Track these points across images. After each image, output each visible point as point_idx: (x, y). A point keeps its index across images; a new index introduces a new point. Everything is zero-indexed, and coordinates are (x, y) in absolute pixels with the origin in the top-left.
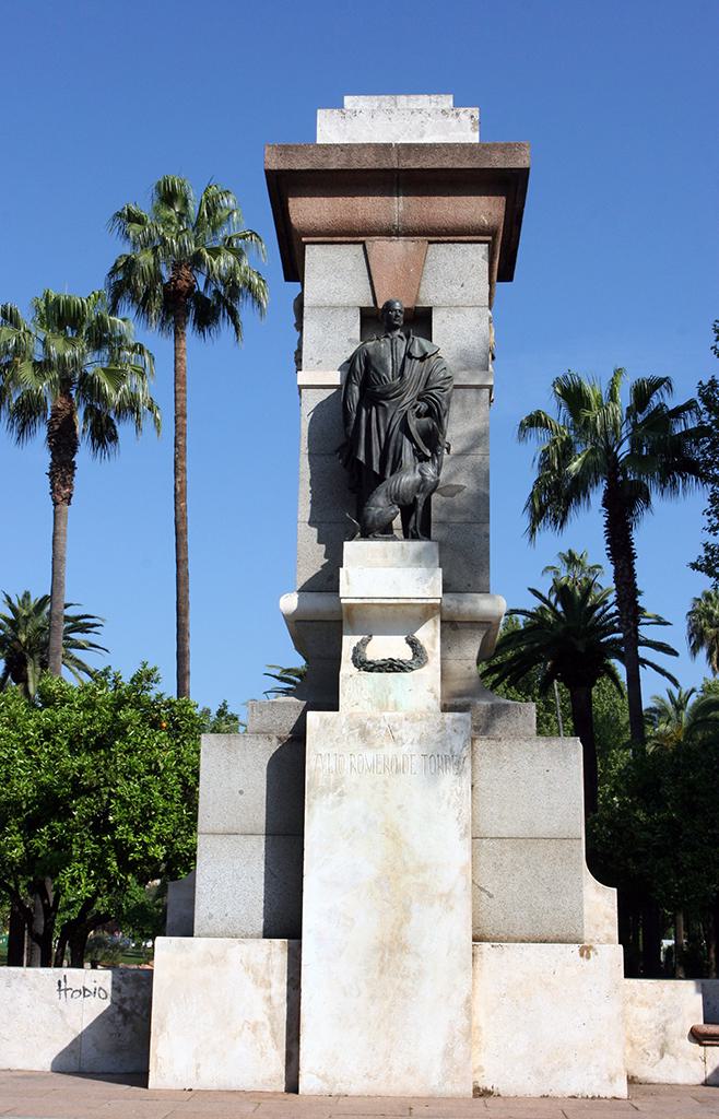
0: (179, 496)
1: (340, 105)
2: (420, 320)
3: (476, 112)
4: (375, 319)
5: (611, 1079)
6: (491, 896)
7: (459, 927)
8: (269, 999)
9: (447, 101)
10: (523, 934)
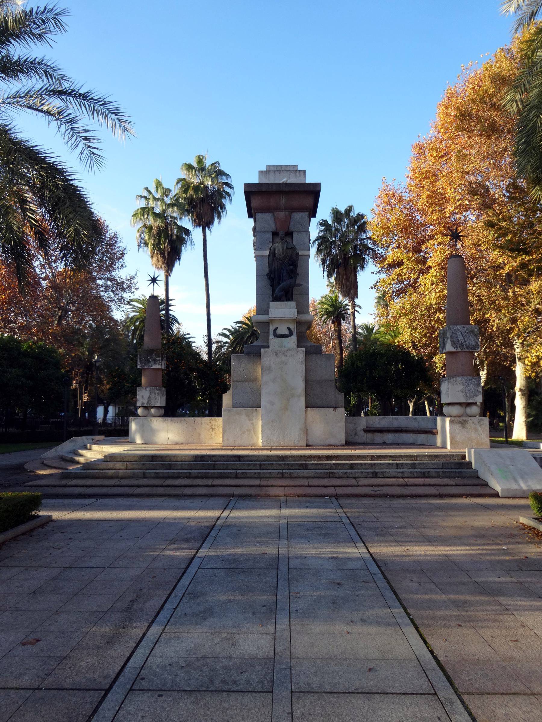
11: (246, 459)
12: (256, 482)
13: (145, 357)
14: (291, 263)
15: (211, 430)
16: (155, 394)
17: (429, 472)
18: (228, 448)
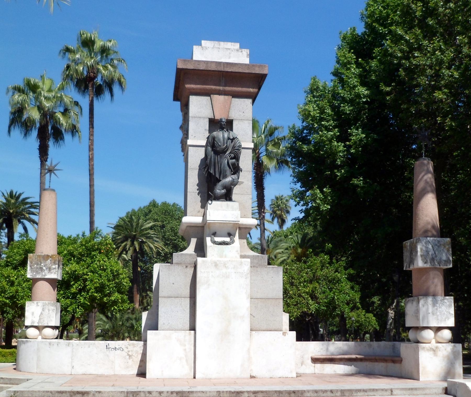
0: (91, 159)
1: (200, 45)
2: (229, 124)
4: (214, 124)
5: (291, 372)
6: (254, 317)
7: (246, 326)
8: (185, 350)
9: (237, 46)
10: (264, 328)
13: (37, 264)
14: (233, 155)
15: (128, 357)
16: (49, 310)
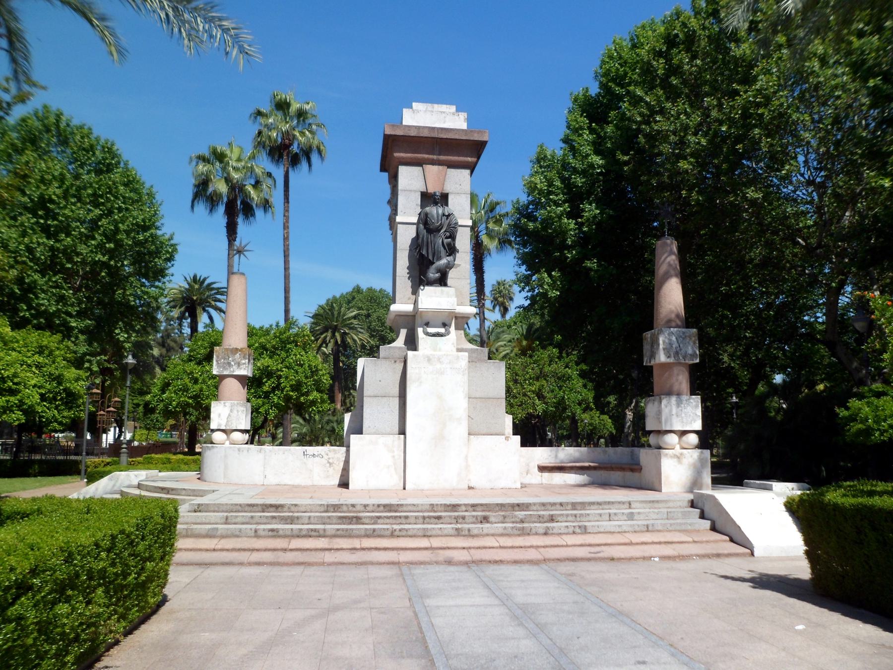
0: (286, 239)
2: (444, 199)
3: (466, 114)
4: (427, 198)
5: (515, 482)
7: (463, 429)
8: (394, 457)
9: (453, 108)
10: (484, 432)
11: (405, 509)
12: (424, 543)
16: (238, 411)
17: (653, 525)
18: (578, 464)
